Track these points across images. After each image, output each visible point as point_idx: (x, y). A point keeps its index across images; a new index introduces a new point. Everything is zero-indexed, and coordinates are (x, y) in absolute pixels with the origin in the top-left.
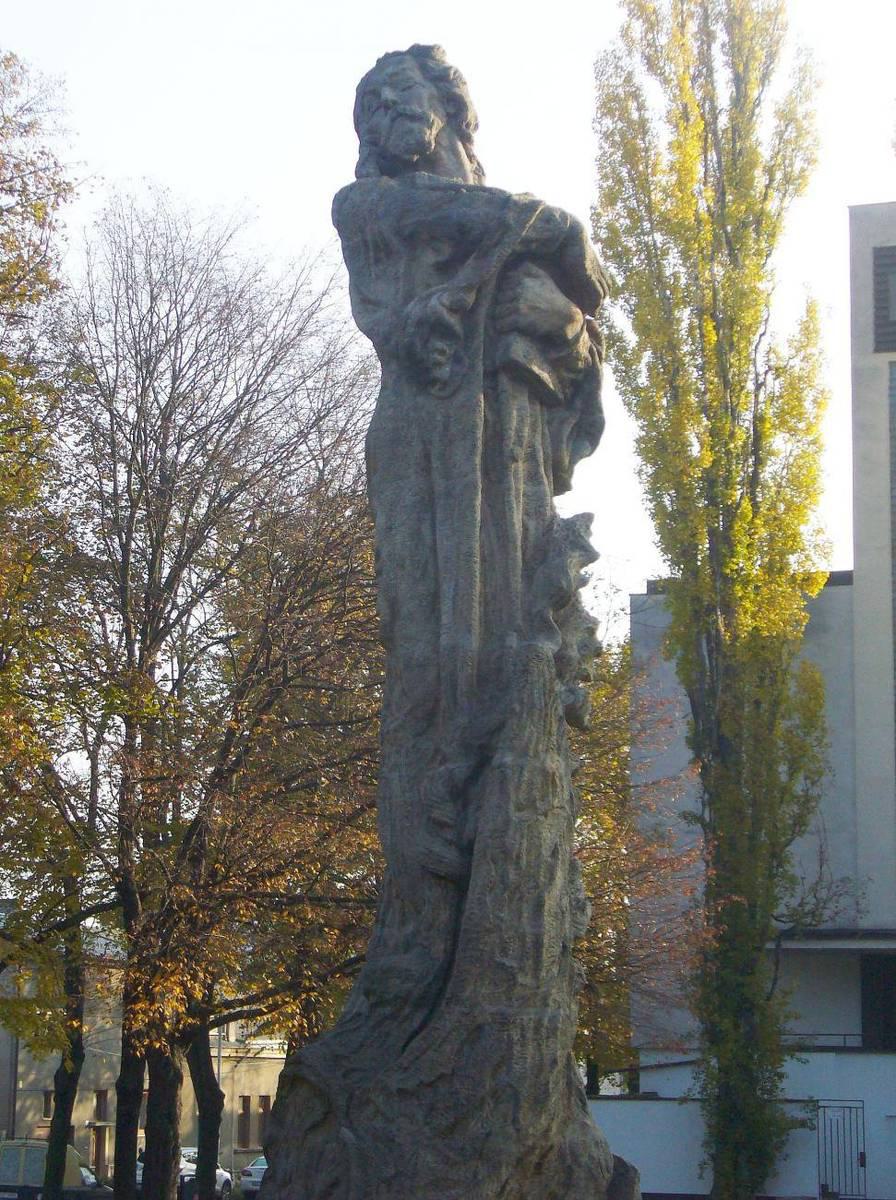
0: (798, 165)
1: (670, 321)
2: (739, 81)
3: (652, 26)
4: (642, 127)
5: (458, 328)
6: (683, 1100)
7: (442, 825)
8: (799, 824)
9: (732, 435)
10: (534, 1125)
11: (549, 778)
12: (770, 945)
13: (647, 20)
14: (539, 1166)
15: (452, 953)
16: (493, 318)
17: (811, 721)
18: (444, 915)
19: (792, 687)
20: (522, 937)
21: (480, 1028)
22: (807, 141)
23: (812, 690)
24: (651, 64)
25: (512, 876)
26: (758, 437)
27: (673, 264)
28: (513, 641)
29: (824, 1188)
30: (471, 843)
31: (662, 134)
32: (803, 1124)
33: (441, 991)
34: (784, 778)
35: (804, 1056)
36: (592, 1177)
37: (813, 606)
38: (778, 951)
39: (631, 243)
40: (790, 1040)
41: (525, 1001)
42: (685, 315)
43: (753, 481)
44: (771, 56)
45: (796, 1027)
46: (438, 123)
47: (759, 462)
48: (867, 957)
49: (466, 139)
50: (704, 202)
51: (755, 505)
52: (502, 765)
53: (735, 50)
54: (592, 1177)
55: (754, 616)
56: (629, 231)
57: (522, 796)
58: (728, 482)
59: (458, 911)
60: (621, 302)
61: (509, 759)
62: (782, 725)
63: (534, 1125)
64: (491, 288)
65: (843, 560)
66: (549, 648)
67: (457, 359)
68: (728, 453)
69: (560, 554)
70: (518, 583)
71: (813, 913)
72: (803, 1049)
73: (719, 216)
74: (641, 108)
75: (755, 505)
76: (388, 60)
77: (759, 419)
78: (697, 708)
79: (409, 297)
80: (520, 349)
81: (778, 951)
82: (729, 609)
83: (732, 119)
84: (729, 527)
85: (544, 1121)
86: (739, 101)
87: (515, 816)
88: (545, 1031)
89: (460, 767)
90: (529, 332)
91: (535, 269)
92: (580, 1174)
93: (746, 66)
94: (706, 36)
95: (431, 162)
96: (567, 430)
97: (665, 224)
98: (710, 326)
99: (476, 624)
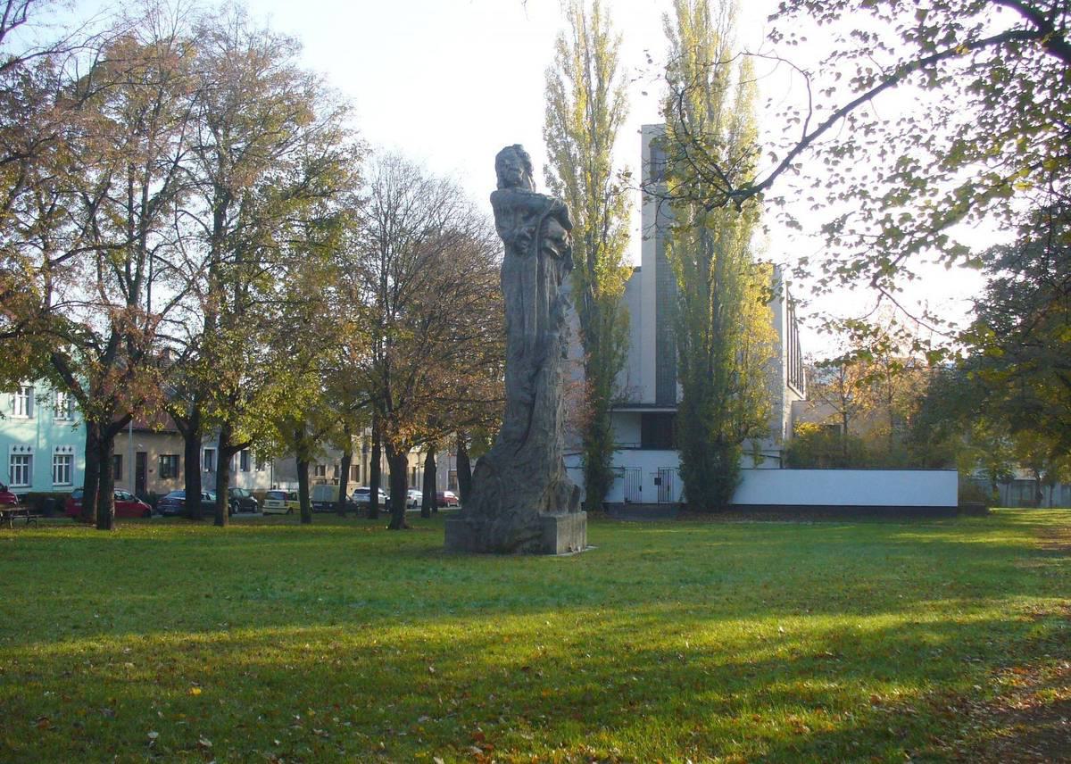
0: (622, 114)
1: (573, 171)
2: (601, 81)
3: (566, 56)
4: (563, 96)
5: (530, 238)
6: (576, 468)
7: (526, 388)
8: (620, 365)
9: (597, 218)
10: (553, 476)
11: (558, 375)
12: (609, 410)
13: (565, 55)
14: (554, 488)
15: (529, 427)
16: (540, 234)
17: (625, 327)
18: (527, 415)
19: (618, 315)
20: (550, 421)
21: (538, 448)
22: (626, 104)
23: (625, 317)
24: (566, 71)
25: (547, 404)
26: (606, 218)
27: (574, 150)
28: (547, 333)
29: (626, 499)
30: (535, 394)
31: (570, 99)
32: (619, 476)
33: (527, 437)
34: (615, 349)
35: (621, 451)
36: (568, 490)
37: (626, 284)
38: (612, 412)
39: (558, 140)
40: (615, 445)
41: (551, 440)
42: (579, 170)
43: (605, 234)
44: (613, 71)
45: (617, 441)
46: (522, 171)
47: (607, 228)
48: (644, 414)
49: (531, 175)
50: (586, 125)
51: (605, 244)
52: (544, 372)
53: (599, 69)
54: (568, 490)
55: (604, 287)
56: (557, 137)
57: (550, 381)
58: (595, 235)
59: (531, 414)
60: (554, 164)
61: (546, 369)
62: (615, 329)
63: (553, 476)
64: (539, 226)
65: (638, 263)
66: (557, 335)
67: (529, 246)
68: (595, 225)
69: (560, 306)
70: (548, 316)
71: (624, 399)
72: (621, 449)
73: (592, 131)
74: (563, 89)
75: (605, 244)
76: (506, 149)
77: (607, 211)
78: (583, 321)
79: (515, 227)
80: (548, 243)
81: (612, 412)
82: (595, 285)
83: (597, 95)
84: (595, 253)
85: (556, 474)
86: (601, 88)
87: (548, 386)
88: (556, 449)
89: (532, 372)
90: (551, 238)
91: (552, 218)
92: (565, 490)
93: (603, 75)
94: (588, 61)
95: (520, 183)
96: (562, 266)
97: (571, 133)
98: (589, 175)
99: (536, 329)
